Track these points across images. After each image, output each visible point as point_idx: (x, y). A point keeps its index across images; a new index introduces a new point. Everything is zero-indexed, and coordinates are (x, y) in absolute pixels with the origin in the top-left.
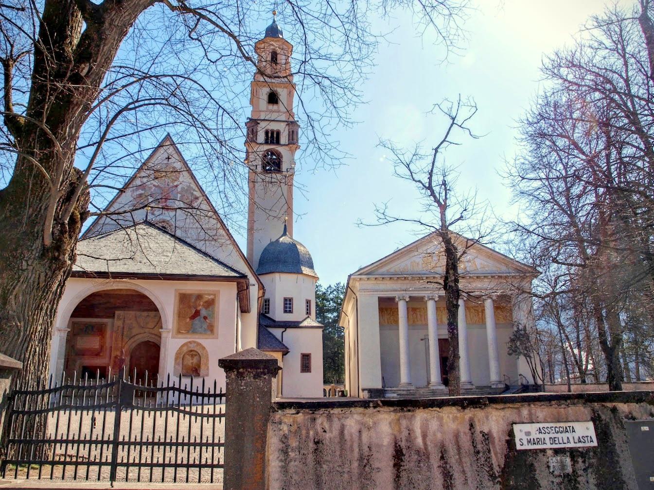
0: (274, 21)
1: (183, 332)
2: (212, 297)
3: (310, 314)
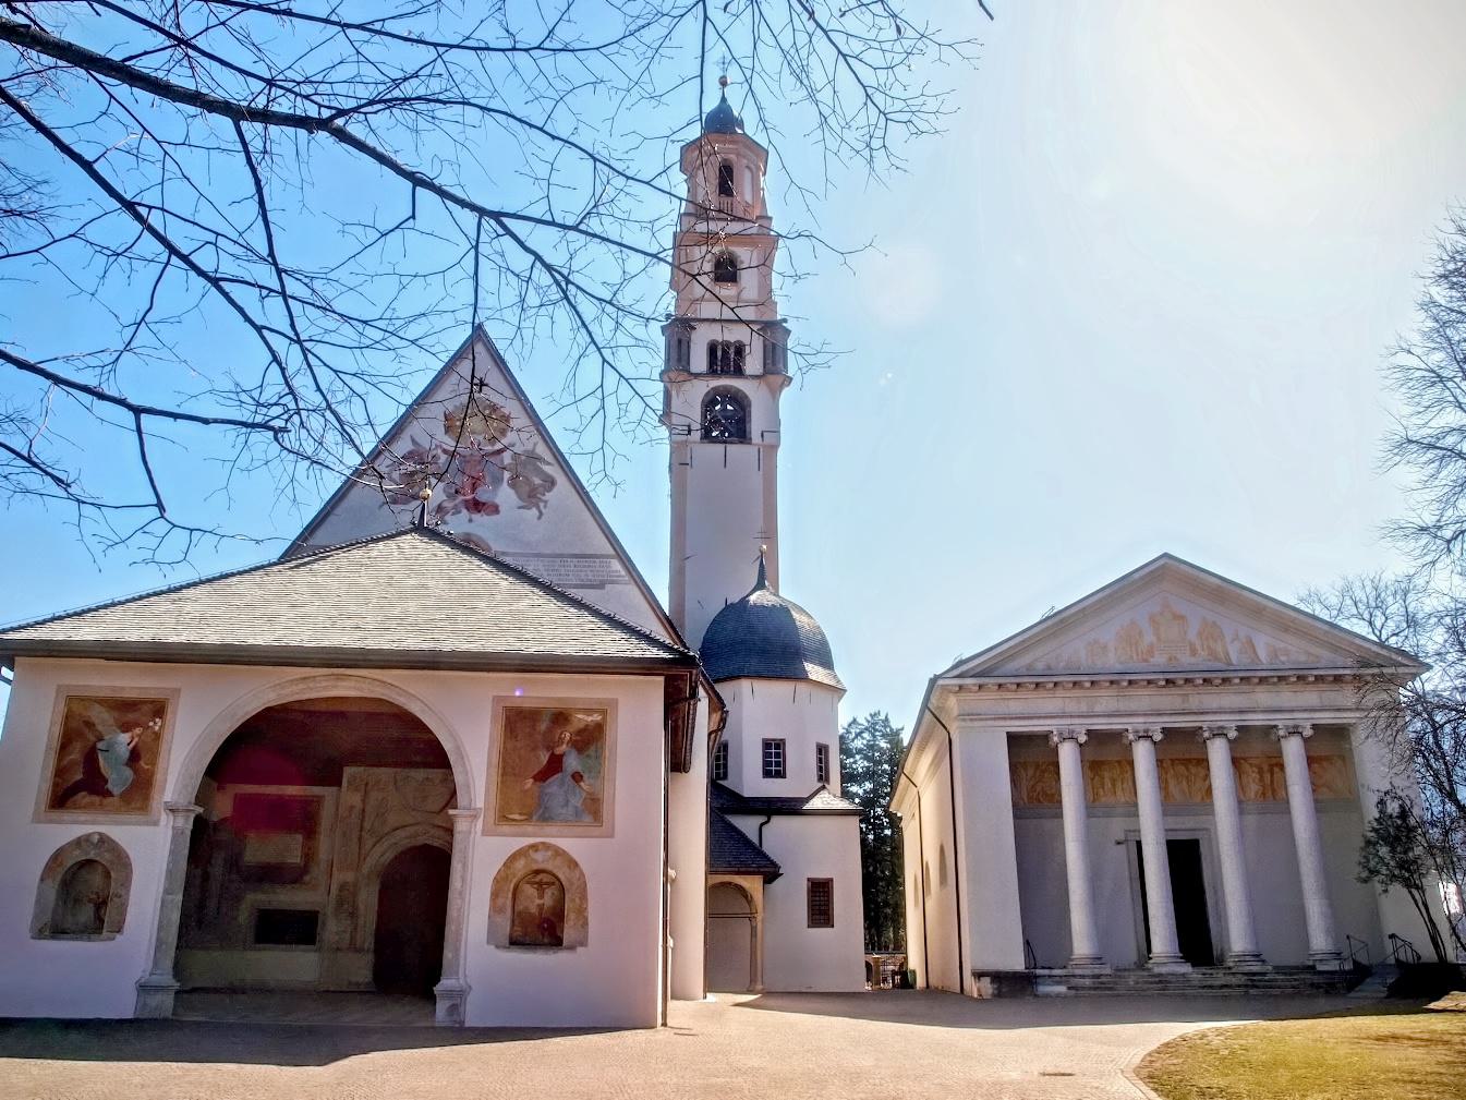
0: (724, 99)
1: (517, 817)
2: (597, 718)
3: (827, 780)
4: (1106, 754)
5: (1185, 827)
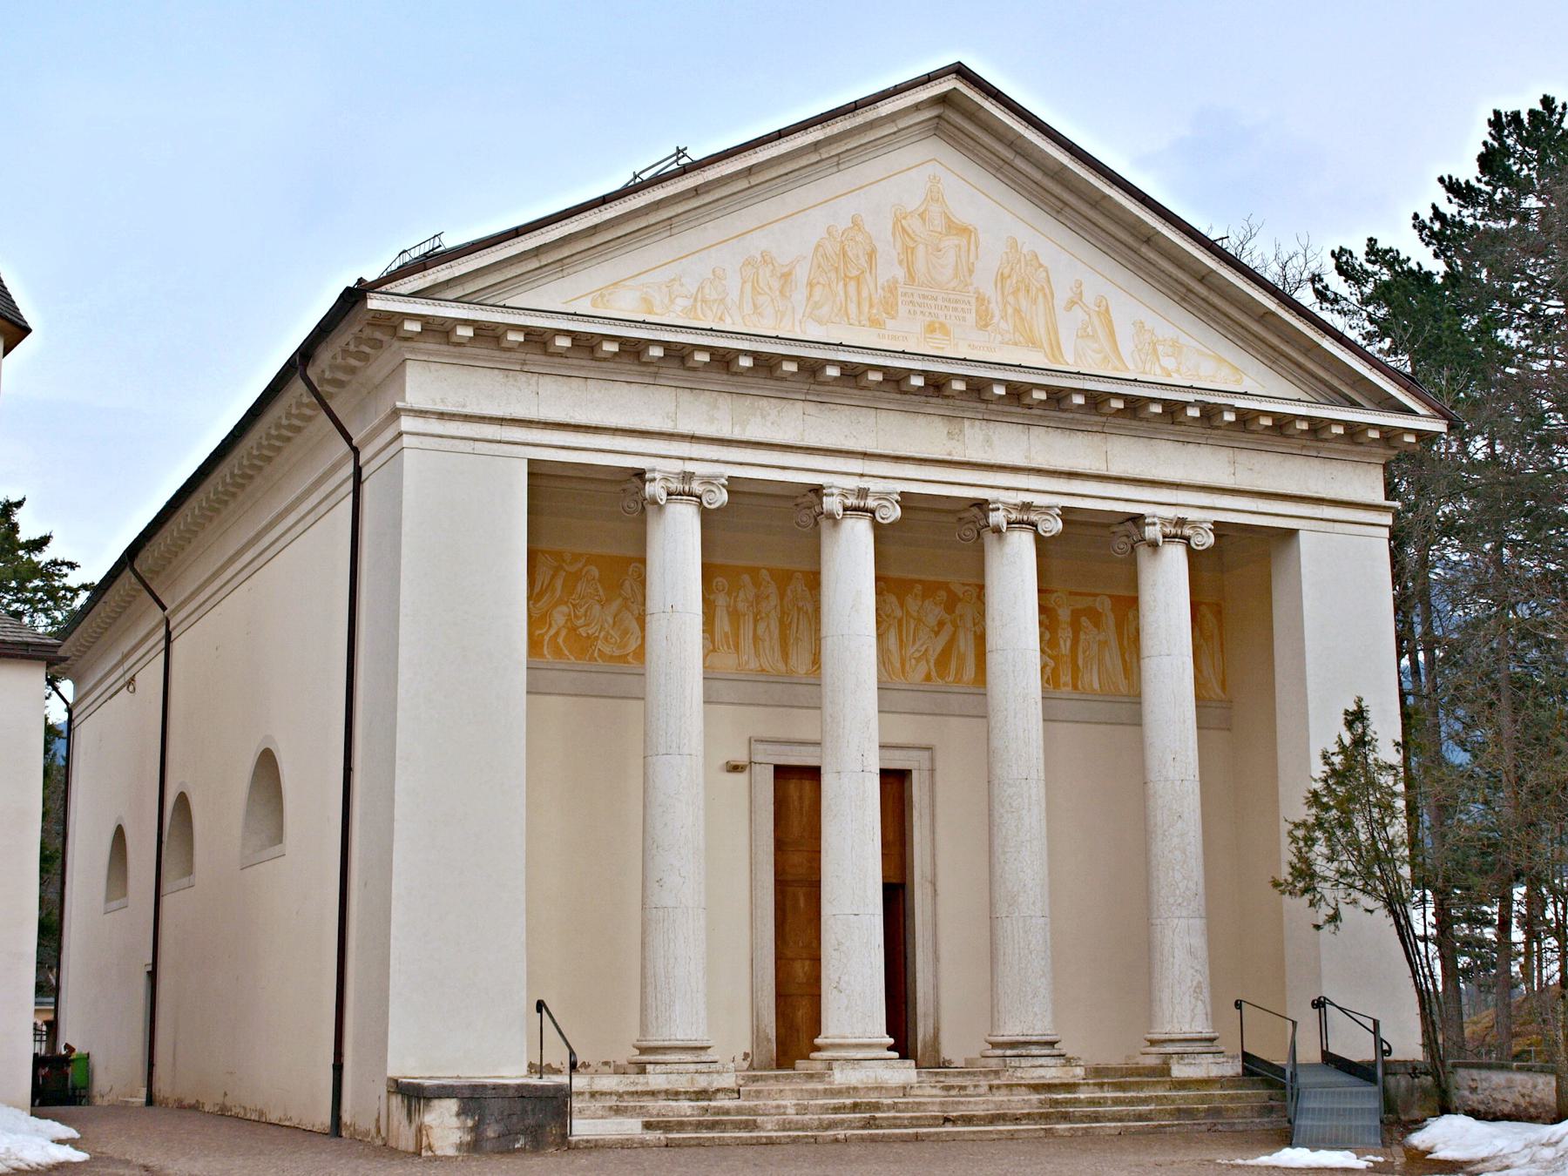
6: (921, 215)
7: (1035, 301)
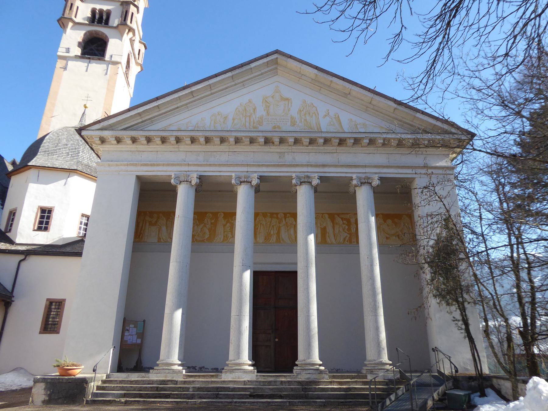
4: (213, 198)
5: (274, 262)
6: (273, 97)
7: (312, 117)
